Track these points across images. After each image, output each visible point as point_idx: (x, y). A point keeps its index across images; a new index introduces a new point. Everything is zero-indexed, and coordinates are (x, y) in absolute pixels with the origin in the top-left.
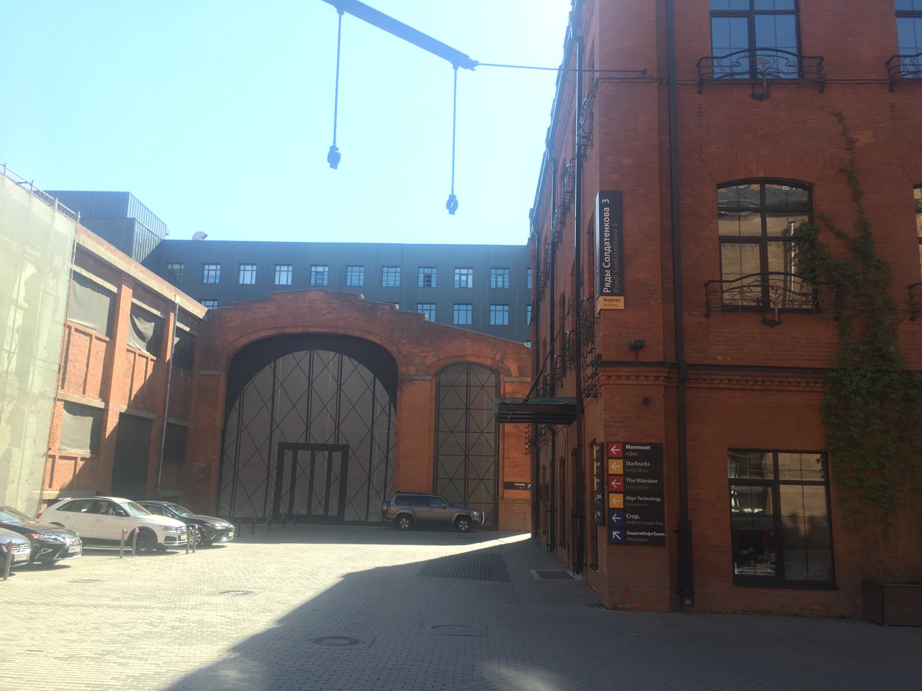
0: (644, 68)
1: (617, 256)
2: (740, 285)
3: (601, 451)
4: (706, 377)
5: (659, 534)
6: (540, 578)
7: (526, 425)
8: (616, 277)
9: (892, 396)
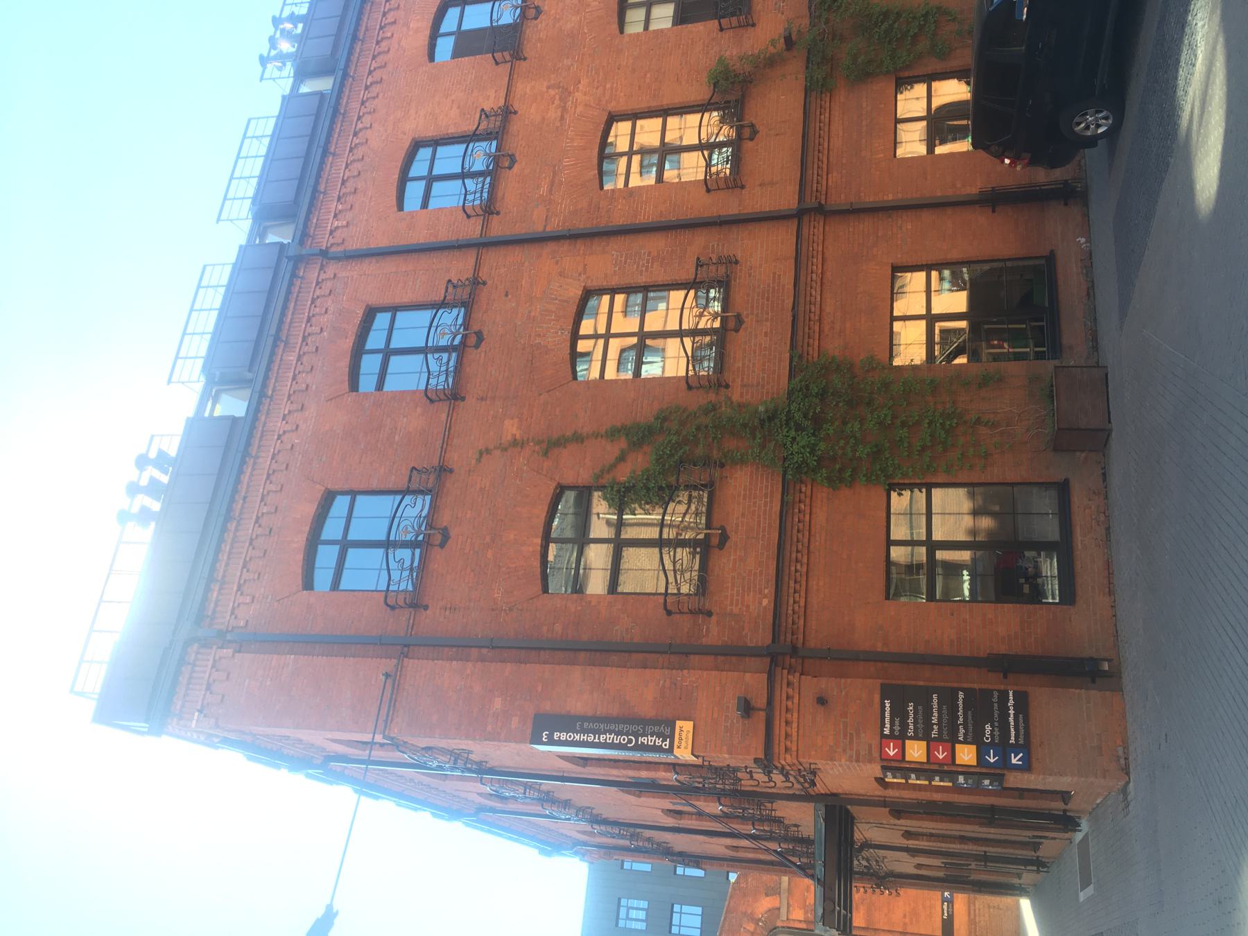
0: (383, 675)
1: (621, 726)
2: (672, 572)
3: (895, 771)
4: (790, 621)
5: (1011, 698)
6: (1092, 886)
7: (854, 890)
8: (649, 729)
9: (818, 409)
